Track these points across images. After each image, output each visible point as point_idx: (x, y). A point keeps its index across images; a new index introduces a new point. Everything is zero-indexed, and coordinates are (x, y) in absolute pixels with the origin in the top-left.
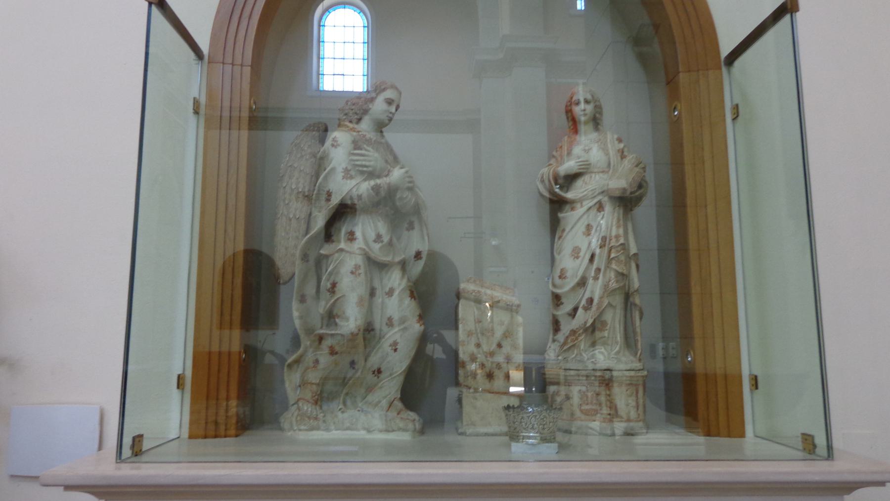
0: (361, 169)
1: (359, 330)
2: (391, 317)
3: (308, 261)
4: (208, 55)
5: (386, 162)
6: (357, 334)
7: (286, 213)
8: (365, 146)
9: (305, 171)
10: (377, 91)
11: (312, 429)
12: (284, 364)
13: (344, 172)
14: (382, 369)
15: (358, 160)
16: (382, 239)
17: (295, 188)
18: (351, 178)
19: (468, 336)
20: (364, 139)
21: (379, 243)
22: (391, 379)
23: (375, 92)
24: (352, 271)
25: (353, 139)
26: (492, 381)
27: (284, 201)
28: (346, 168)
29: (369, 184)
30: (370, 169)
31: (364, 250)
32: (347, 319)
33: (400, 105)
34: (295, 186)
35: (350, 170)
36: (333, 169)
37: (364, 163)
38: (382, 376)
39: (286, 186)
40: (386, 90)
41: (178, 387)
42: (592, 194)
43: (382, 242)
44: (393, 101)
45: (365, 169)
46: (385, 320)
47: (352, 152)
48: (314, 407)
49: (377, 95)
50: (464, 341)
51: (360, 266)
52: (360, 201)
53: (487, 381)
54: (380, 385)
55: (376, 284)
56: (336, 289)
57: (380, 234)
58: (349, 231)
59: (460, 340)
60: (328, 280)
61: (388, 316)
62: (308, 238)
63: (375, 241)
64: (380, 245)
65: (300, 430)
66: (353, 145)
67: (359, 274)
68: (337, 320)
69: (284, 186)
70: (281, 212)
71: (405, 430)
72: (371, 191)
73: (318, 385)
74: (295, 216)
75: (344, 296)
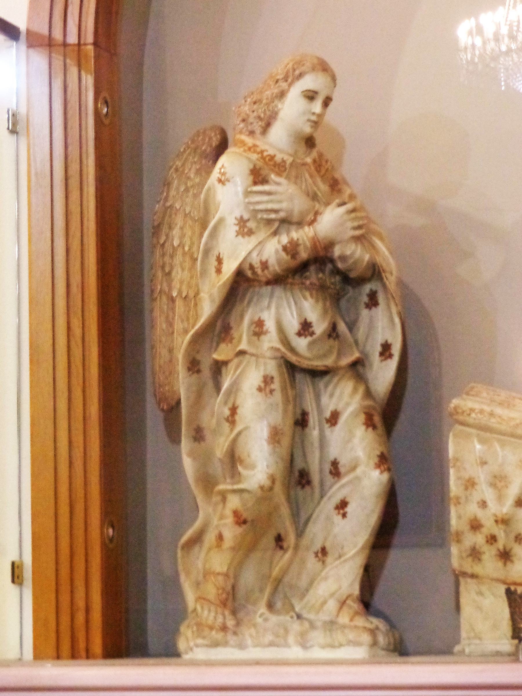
0: (265, 216)
1: (273, 481)
2: (335, 459)
3: (199, 371)
4: (25, 32)
5: (314, 197)
6: (271, 489)
7: (167, 289)
8: (273, 176)
9: (192, 214)
10: (290, 80)
11: (215, 644)
12: (176, 547)
13: (237, 225)
14: (328, 549)
15: (258, 203)
16: (311, 330)
17: (179, 246)
18: (250, 233)
19: (466, 489)
20: (272, 163)
21: (306, 337)
22: (341, 563)
23: (287, 81)
24: (260, 386)
25: (251, 167)
26: (508, 563)
27: (163, 267)
28: (242, 217)
29: (279, 242)
30: (282, 215)
31: (278, 350)
32: (253, 467)
33: (334, 98)
34: (178, 242)
35: (248, 220)
36: (221, 221)
37: (270, 206)
38: (329, 559)
39: (165, 242)
40: (303, 76)
41: (13, 581)
42: (160, 352)
43: (312, 334)
44: (316, 93)
45: (273, 216)
46: (327, 467)
47: (249, 189)
48: (219, 610)
49: (290, 85)
50: (458, 498)
51: (272, 378)
52: (266, 272)
53: (500, 564)
54: (323, 574)
55: (310, 406)
56: (237, 418)
57: (309, 320)
58: (256, 319)
59: (452, 494)
60: (226, 403)
61: (332, 458)
62: (193, 336)
63: (299, 334)
64: (309, 339)
65: (197, 646)
66: (251, 178)
67: (272, 391)
68: (240, 468)
69: (162, 241)
70: (159, 287)
71: (357, 644)
72: (284, 254)
73: (226, 575)
74: (180, 292)
75: (246, 428)
